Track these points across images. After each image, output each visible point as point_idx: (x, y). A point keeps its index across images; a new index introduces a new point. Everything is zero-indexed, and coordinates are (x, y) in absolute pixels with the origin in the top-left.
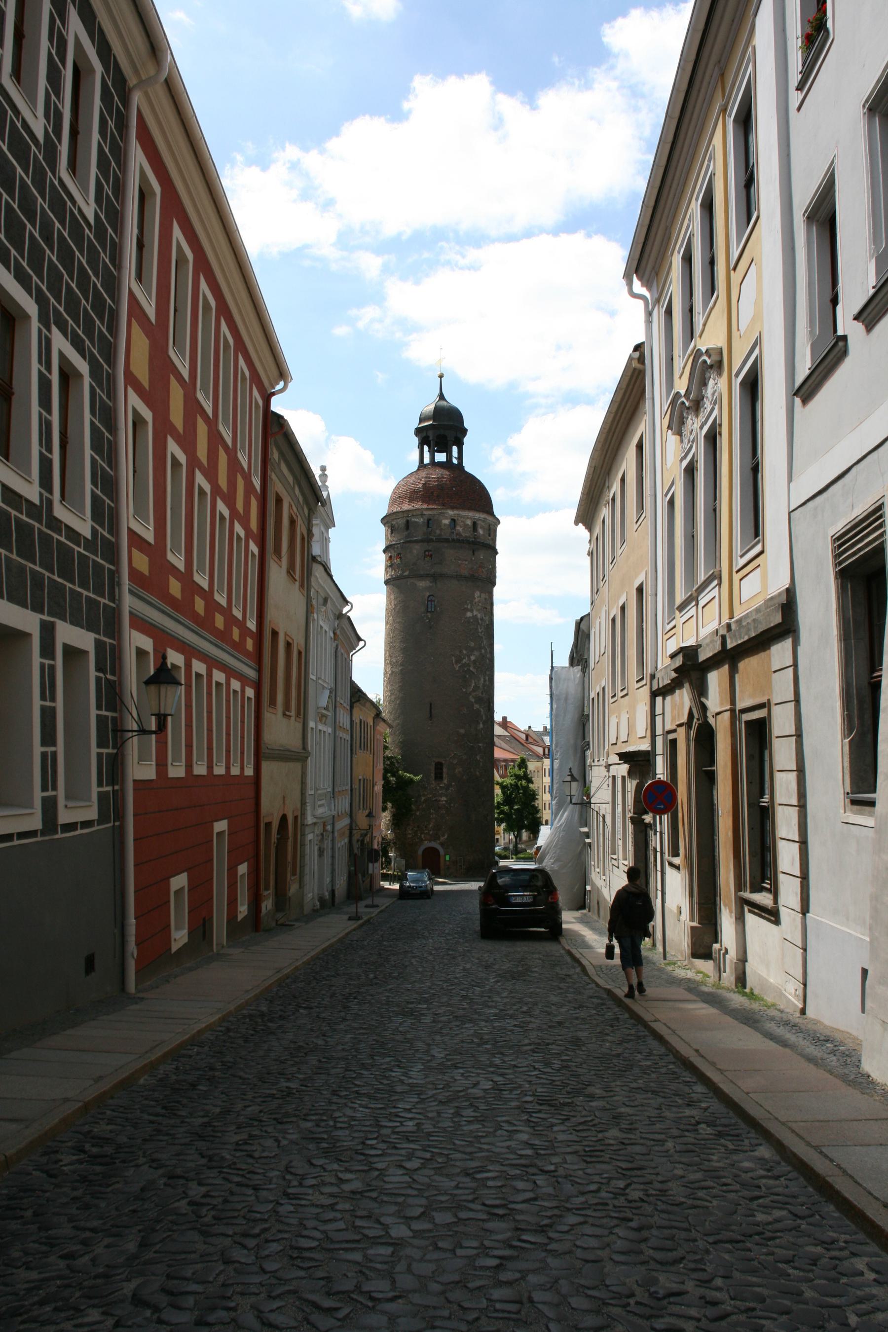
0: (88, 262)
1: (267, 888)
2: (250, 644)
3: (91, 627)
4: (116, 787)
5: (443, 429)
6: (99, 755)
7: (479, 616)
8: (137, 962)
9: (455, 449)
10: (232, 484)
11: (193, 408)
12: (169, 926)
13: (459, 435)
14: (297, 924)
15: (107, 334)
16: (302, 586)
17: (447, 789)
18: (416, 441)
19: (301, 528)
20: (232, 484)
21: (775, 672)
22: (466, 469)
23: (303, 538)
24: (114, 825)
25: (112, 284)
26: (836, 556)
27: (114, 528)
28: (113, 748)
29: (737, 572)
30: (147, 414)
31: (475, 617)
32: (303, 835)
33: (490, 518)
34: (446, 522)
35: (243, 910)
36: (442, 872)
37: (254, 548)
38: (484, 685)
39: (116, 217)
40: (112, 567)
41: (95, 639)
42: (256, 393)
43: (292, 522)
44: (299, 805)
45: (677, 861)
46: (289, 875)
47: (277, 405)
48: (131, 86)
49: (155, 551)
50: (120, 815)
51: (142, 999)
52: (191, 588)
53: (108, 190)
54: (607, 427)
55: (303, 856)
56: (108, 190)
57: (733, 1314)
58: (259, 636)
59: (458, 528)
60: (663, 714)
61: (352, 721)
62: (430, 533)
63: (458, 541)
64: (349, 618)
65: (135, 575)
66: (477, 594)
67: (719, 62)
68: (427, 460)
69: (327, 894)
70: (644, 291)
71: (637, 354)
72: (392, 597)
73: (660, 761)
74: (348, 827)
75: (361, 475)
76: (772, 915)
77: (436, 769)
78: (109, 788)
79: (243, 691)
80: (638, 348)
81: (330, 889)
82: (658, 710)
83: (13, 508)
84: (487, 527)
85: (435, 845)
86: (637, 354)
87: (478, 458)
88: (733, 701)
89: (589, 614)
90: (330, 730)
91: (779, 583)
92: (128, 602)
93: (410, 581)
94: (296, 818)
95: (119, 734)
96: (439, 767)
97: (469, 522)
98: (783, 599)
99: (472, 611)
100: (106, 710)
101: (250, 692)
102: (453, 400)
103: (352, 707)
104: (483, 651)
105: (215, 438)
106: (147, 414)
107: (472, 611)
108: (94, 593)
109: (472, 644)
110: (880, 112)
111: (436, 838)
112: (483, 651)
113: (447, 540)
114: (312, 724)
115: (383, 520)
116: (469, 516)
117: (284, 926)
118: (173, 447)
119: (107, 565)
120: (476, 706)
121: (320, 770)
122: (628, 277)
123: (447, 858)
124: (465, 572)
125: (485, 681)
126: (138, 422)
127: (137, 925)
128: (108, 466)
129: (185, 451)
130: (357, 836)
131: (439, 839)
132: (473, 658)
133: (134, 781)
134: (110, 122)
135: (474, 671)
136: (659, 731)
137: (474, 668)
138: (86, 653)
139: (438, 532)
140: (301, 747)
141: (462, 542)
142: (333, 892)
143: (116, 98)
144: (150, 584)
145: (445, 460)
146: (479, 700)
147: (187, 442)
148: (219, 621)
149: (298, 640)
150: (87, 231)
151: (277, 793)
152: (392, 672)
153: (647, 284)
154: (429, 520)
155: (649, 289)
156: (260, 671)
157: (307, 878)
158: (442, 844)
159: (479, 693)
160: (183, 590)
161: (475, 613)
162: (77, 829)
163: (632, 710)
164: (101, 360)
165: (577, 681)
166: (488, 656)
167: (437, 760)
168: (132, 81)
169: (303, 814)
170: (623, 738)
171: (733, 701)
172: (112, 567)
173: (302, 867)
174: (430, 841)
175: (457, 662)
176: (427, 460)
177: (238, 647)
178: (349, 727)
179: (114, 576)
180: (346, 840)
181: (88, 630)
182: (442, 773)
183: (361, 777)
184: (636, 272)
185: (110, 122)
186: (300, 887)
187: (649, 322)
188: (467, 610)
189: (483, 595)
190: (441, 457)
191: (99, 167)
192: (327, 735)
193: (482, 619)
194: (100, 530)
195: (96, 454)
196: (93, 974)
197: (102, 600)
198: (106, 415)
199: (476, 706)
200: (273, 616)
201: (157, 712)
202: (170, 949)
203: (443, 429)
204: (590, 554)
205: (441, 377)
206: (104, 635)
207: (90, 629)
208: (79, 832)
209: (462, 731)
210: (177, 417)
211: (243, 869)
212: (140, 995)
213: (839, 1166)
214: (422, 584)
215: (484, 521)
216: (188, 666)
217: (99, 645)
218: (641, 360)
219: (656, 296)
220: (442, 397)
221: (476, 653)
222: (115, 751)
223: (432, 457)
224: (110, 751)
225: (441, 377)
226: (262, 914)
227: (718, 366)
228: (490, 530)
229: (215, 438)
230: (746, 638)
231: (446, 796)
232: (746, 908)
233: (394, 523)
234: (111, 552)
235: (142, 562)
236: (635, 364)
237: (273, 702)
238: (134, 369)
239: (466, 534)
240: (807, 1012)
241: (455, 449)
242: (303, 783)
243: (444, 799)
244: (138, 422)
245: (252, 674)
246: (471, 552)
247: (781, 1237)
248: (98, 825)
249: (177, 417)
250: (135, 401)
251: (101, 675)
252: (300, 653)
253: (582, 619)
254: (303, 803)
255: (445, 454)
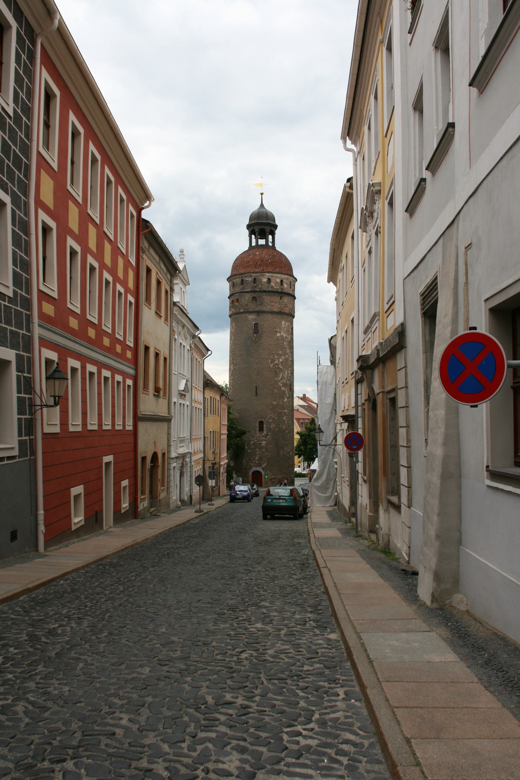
0: (9, 138)
1: (143, 493)
2: (129, 354)
3: (13, 346)
4: (31, 437)
5: (262, 225)
6: (19, 420)
7: (284, 336)
8: (45, 535)
9: (270, 237)
10: (115, 262)
11: (85, 219)
12: (70, 515)
13: (273, 229)
14: (163, 515)
15: (23, 178)
16: (166, 319)
17: (266, 437)
18: (247, 232)
19: (165, 286)
20: (115, 262)
21: (399, 370)
22: (277, 249)
23: (167, 292)
24: (30, 459)
25: (26, 150)
26: (422, 304)
27: (29, 290)
28: (29, 415)
29: (386, 312)
30: (52, 224)
31: (282, 336)
32: (169, 464)
33: (291, 278)
34: (265, 280)
35: (125, 505)
36: (264, 485)
37: (131, 299)
38: (287, 376)
39: (28, 111)
40: (28, 313)
41: (16, 353)
42: (131, 208)
43: (159, 283)
44: (166, 446)
45: (365, 478)
46: (159, 487)
47: (145, 214)
48: (37, 33)
49: (59, 303)
50: (34, 453)
51: (47, 555)
52: (85, 323)
53: (22, 95)
54: (338, 226)
55: (169, 476)
56: (22, 95)
57: (404, 735)
58: (135, 350)
59: (272, 284)
60: (361, 394)
61: (204, 398)
62: (255, 287)
63: (272, 292)
64: (199, 338)
65: (42, 316)
66: (283, 322)
67: (379, 14)
68: (254, 244)
69: (186, 497)
70: (353, 147)
71: (349, 184)
72: (234, 324)
73: (360, 420)
74: (202, 459)
75: (208, 254)
76: (397, 508)
77: (260, 425)
78: (27, 438)
79: (124, 381)
80: (349, 180)
81: (189, 494)
82: (359, 392)
83: (24, 273)
84: (289, 283)
85: (259, 469)
86: (349, 184)
87: (284, 242)
88: (383, 387)
89: (336, 335)
90: (188, 403)
91: (400, 320)
92: (37, 331)
93: (244, 315)
94: (164, 454)
95: (33, 407)
96: (261, 423)
97: (278, 280)
98: (400, 330)
99: (280, 333)
100: (24, 394)
101: (129, 382)
102: (269, 207)
103: (204, 389)
104: (287, 356)
105: (102, 236)
106: (52, 224)
107: (280, 333)
108: (15, 328)
109: (280, 352)
110: (441, 49)
111: (260, 465)
112: (287, 356)
113: (265, 291)
114: (174, 399)
115: (228, 279)
116: (277, 278)
117: (155, 516)
118: (71, 242)
119: (24, 312)
120: (283, 389)
121: (180, 428)
122: (344, 138)
123: (266, 477)
124: (276, 310)
125: (288, 373)
126: (46, 230)
127: (45, 515)
128: (25, 255)
129: (80, 244)
130: (208, 464)
131: (261, 466)
132: (281, 360)
133: (44, 434)
134: (23, 56)
135: (281, 368)
136: (359, 404)
137: (282, 366)
138: (10, 362)
139: (260, 286)
140: (167, 412)
141: (274, 292)
142: (191, 496)
143: (27, 41)
144: (58, 321)
145: (264, 243)
146: (285, 385)
147: (82, 238)
148: (106, 342)
149: (164, 351)
150: (8, 120)
151: (149, 440)
152: (234, 369)
153: (354, 143)
154: (255, 279)
155: (356, 146)
156: (136, 370)
157: (172, 489)
158: (263, 469)
159: (284, 381)
160: (79, 325)
161: (282, 334)
162: (4, 461)
163: (350, 393)
164: (19, 194)
165: (332, 375)
166: (290, 359)
167: (260, 420)
168: (37, 30)
169: (169, 452)
170: (346, 408)
171: (383, 387)
172: (28, 313)
173: (169, 482)
174: (256, 467)
175: (271, 363)
176: (254, 244)
177: (121, 356)
178: (202, 401)
179: (29, 318)
180: (201, 467)
181: (11, 349)
182: (263, 428)
183: (211, 430)
184: (348, 135)
185: (23, 56)
186: (167, 494)
187: (355, 165)
188: (277, 332)
189: (287, 324)
190: (262, 242)
191: (16, 82)
192: (186, 406)
193: (286, 337)
194: (19, 291)
195: (16, 248)
196: (16, 541)
197: (21, 332)
198: (23, 226)
199: (283, 389)
200: (146, 338)
201: (53, 394)
202: (71, 528)
203: (262, 225)
204: (336, 299)
205: (262, 194)
206: (23, 351)
207: (12, 348)
208: (6, 462)
209: (275, 403)
210: (74, 223)
211: (125, 483)
212: (46, 554)
213: (363, 644)
214: (251, 317)
215: (287, 280)
216: (84, 368)
217: (19, 358)
218: (351, 187)
219: (359, 150)
220: (262, 205)
221: (283, 357)
222: (30, 417)
223: (257, 242)
224: (27, 417)
225: (262, 194)
226: (139, 510)
227: (379, 192)
228: (291, 285)
229: (102, 236)
230: (387, 351)
231: (265, 441)
232: (389, 505)
233: (234, 281)
234: (27, 304)
235: (49, 309)
236: (348, 190)
237: (146, 386)
238: (42, 198)
239: (277, 287)
240: (411, 562)
241: (270, 237)
242: (169, 434)
243: (265, 442)
244: (46, 230)
245: (132, 372)
246: (279, 298)
247: (309, 678)
248: (19, 458)
249: (74, 223)
250: (43, 216)
251: (20, 374)
252: (165, 359)
253: (332, 338)
254: (169, 446)
255: (264, 240)
